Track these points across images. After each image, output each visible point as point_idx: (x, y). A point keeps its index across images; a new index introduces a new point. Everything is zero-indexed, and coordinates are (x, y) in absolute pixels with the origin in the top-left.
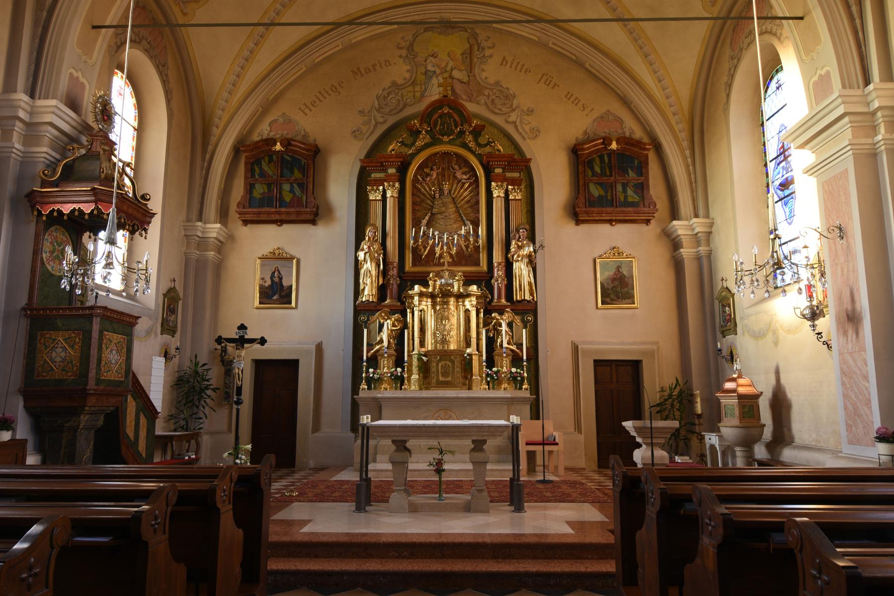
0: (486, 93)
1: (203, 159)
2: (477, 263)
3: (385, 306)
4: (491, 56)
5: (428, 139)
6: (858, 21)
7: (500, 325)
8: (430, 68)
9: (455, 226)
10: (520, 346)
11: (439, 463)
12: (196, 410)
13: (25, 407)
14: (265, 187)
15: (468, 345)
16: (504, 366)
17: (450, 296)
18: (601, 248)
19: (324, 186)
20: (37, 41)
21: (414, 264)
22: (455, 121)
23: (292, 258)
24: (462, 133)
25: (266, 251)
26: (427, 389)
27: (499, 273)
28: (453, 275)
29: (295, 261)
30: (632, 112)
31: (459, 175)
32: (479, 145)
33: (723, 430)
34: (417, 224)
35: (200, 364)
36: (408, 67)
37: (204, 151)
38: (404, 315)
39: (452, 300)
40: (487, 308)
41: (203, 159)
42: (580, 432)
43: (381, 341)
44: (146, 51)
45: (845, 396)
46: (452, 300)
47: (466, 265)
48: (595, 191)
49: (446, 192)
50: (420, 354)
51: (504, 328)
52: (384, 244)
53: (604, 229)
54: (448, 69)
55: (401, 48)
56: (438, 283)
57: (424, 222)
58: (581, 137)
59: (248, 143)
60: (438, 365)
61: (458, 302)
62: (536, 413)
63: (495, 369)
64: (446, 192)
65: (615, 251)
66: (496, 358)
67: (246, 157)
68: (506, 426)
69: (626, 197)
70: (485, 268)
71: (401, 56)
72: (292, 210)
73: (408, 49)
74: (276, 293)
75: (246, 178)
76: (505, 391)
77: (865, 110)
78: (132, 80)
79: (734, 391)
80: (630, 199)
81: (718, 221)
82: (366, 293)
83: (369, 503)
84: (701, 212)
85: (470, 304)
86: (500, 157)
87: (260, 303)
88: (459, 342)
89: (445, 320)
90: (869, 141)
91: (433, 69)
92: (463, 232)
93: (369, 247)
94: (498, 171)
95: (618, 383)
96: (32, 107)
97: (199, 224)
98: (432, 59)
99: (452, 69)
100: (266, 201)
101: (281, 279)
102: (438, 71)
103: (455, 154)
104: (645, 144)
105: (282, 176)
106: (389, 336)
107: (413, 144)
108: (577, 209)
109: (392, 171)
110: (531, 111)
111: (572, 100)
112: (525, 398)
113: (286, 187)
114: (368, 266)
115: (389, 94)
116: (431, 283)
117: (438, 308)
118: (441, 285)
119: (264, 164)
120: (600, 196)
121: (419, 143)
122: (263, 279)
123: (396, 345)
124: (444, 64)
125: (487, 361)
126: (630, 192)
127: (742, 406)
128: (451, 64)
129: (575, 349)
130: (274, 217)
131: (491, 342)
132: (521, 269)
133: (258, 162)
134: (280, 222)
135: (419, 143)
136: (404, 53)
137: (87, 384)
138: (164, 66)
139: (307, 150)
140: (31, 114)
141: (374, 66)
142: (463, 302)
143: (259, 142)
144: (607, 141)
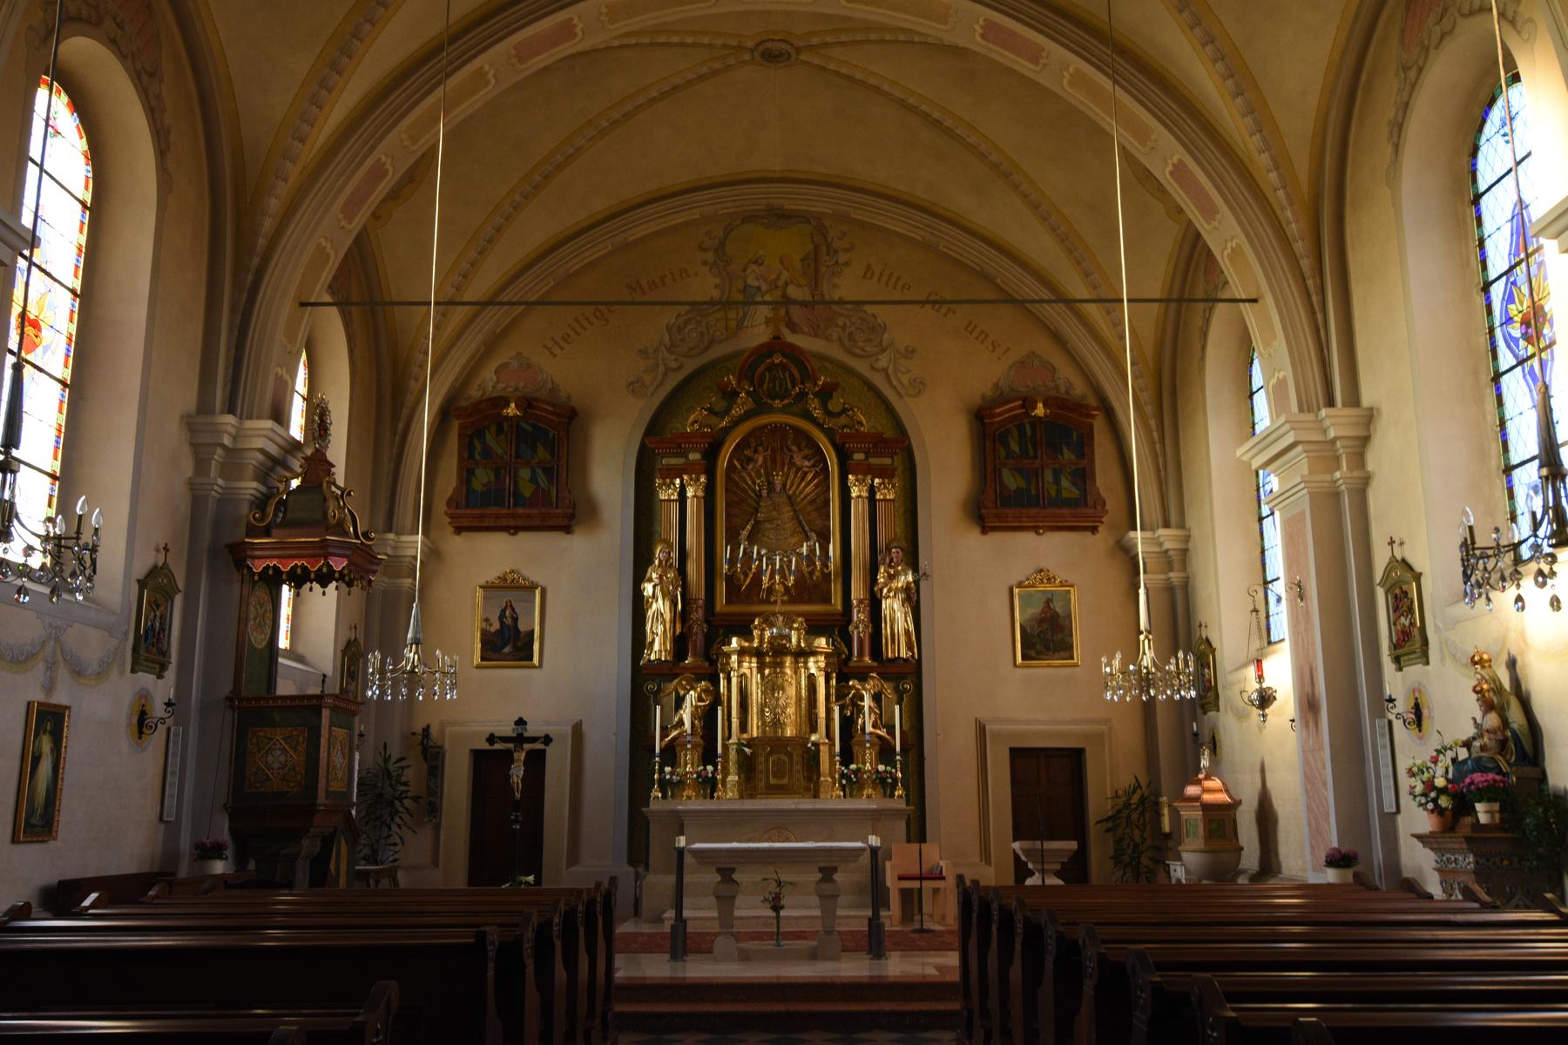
0: (840, 322)
1: (394, 432)
2: (826, 599)
3: (686, 668)
4: (847, 264)
5: (750, 404)
6: (1319, 316)
7: (862, 699)
8: (752, 281)
9: (793, 540)
10: (891, 729)
11: (777, 898)
12: (385, 831)
13: (230, 828)
14: (492, 475)
15: (814, 729)
16: (868, 762)
17: (786, 654)
18: (1021, 569)
19: (583, 470)
20: (236, 333)
21: (729, 601)
22: (791, 375)
23: (533, 587)
24: (802, 395)
25: (491, 575)
26: (752, 797)
27: (859, 616)
28: (789, 623)
29: (538, 592)
30: (1068, 351)
31: (798, 460)
32: (828, 413)
33: (1185, 855)
34: (733, 539)
35: (393, 759)
36: (718, 281)
37: (395, 418)
38: (716, 683)
39: (788, 661)
40: (842, 671)
41: (394, 432)
42: (988, 862)
43: (681, 723)
44: (112, 43)
45: (1309, 808)
46: (788, 661)
47: (810, 602)
48: (1011, 481)
49: (778, 488)
50: (740, 744)
51: (867, 702)
52: (682, 571)
53: (1026, 539)
54: (781, 283)
55: (704, 250)
56: (767, 634)
57: (745, 533)
58: (989, 394)
59: (463, 404)
60: (767, 760)
61: (797, 662)
62: (918, 830)
63: (853, 767)
64: (778, 488)
65: (1043, 574)
66: (855, 749)
67: (461, 427)
68: (862, 850)
69: (1059, 492)
70: (839, 607)
71: (705, 263)
72: (535, 511)
73: (716, 250)
74: (508, 643)
75: (461, 459)
76: (868, 801)
77: (1320, 438)
78: (81, 105)
79: (1197, 799)
80: (1065, 495)
81: (1195, 533)
82: (656, 647)
83: (685, 952)
84: (1173, 518)
85: (815, 666)
86: (862, 437)
87: (483, 659)
88: (798, 725)
89: (778, 688)
90: (1328, 478)
91: (756, 284)
92: (804, 550)
93: (660, 578)
94: (858, 456)
95: (1046, 782)
96: (238, 429)
97: (391, 536)
98: (754, 267)
99: (786, 284)
100: (492, 497)
101: (515, 620)
102: (764, 287)
103: (793, 427)
104: (1087, 407)
105: (518, 456)
106: (693, 716)
107: (727, 412)
108: (983, 511)
109: (694, 456)
110: (910, 353)
111: (975, 334)
112: (898, 810)
113: (525, 473)
114: (659, 606)
115: (686, 323)
116: (756, 633)
117: (767, 672)
118: (772, 637)
119: (488, 436)
120: (1019, 490)
121: (736, 411)
122: (487, 620)
123: (703, 728)
124: (773, 277)
125: (842, 753)
126: (1065, 483)
127: (1208, 821)
128: (785, 275)
129: (981, 730)
130: (505, 522)
131: (848, 724)
132: (895, 610)
133: (479, 434)
134: (514, 530)
135: (736, 411)
136: (710, 257)
137: (316, 798)
138: (152, 75)
139: (558, 415)
140: (235, 438)
141: (662, 278)
142: (806, 663)
143: (480, 402)
144: (1029, 403)
